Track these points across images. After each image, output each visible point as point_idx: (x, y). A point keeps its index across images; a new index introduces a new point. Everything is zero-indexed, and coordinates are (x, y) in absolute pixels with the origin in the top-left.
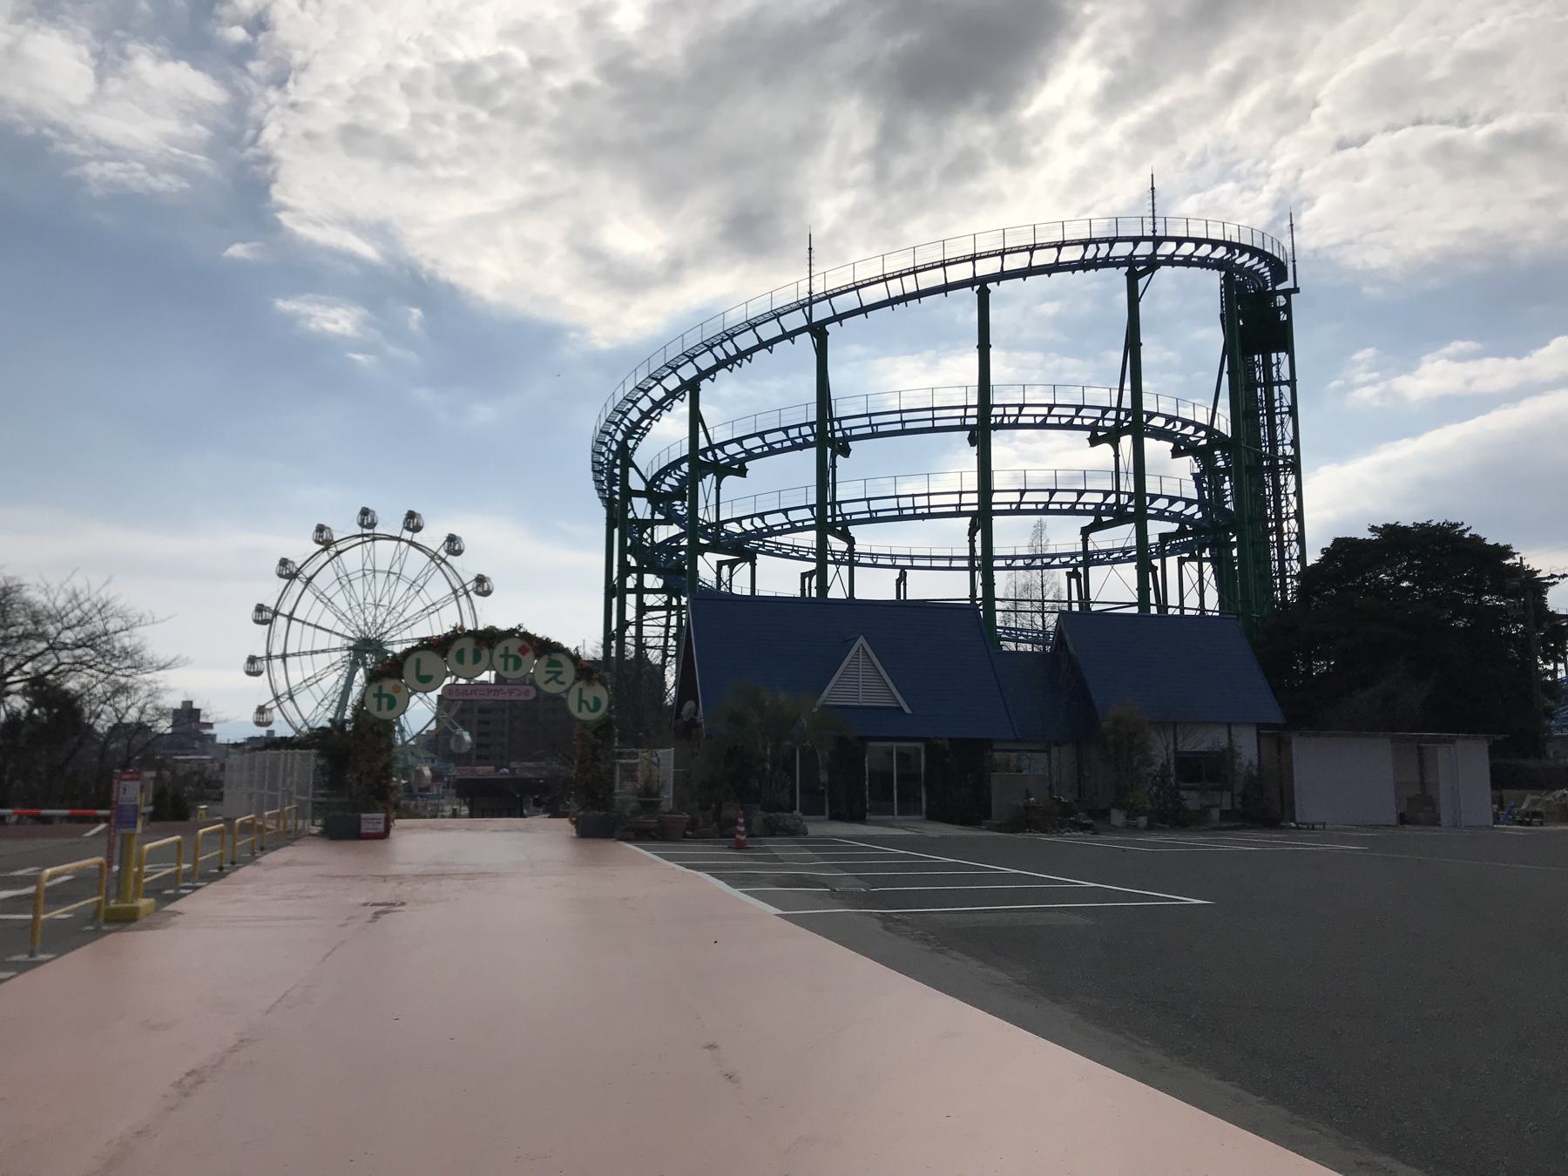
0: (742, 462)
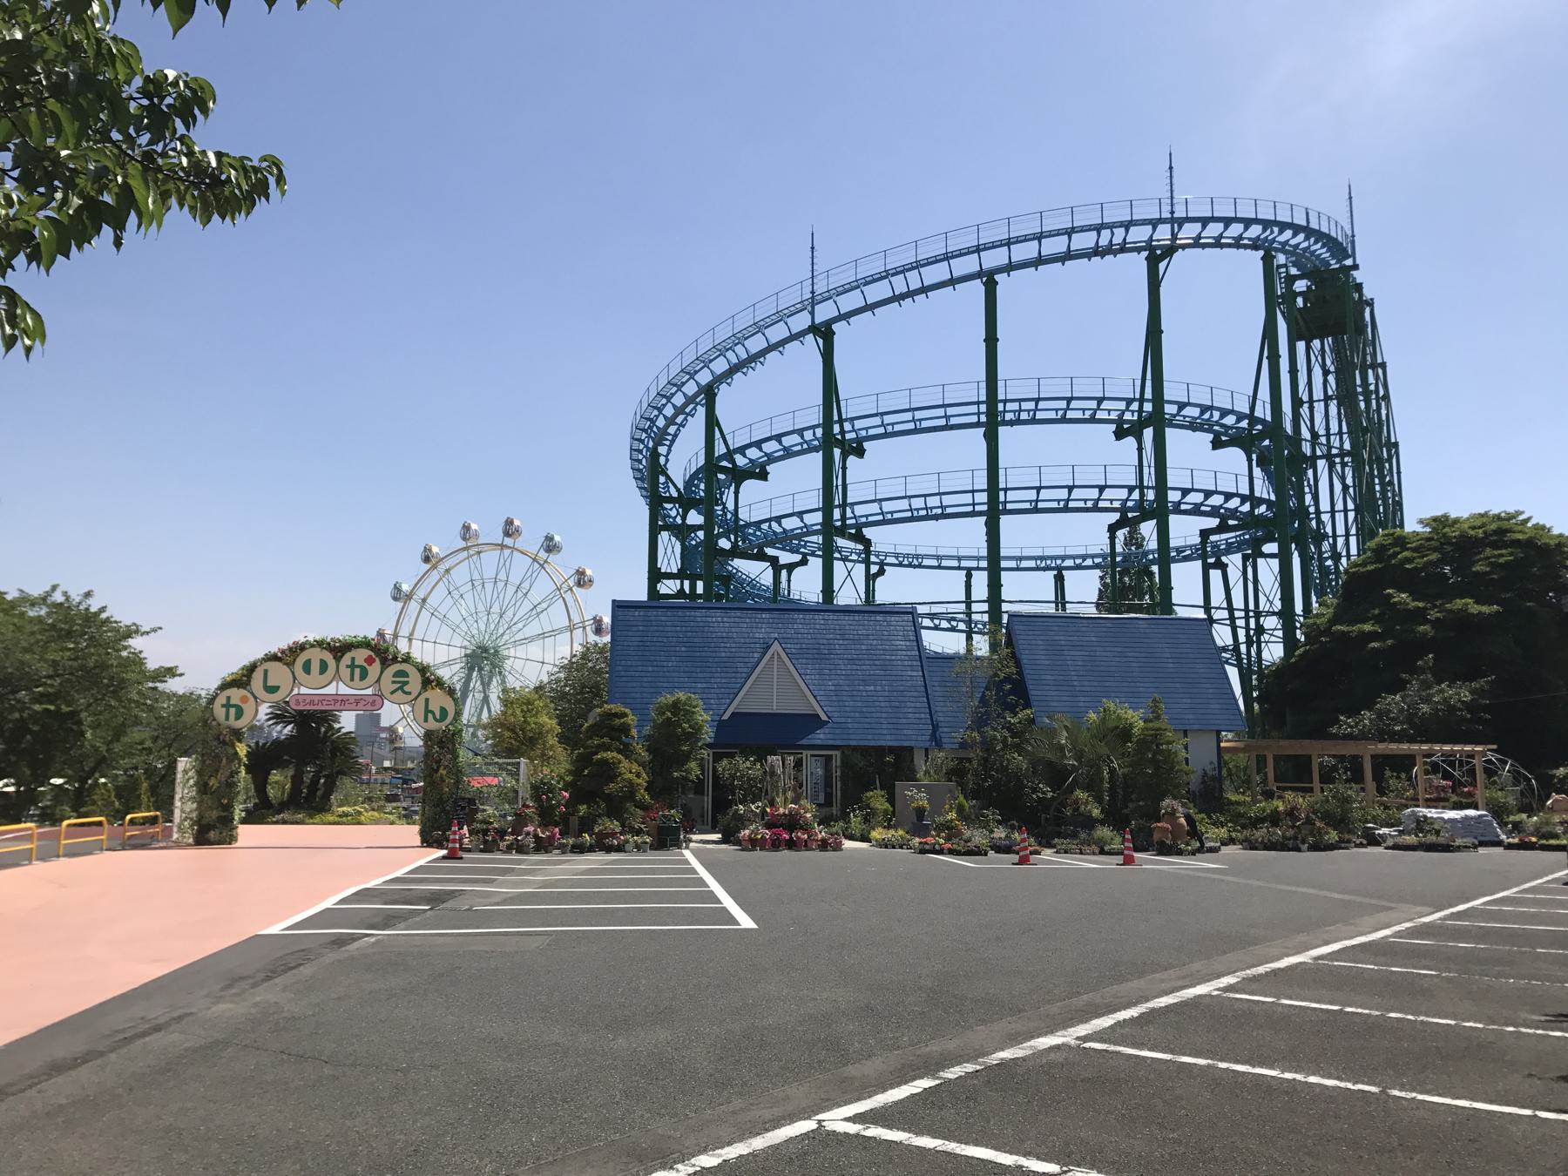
0: (763, 467)
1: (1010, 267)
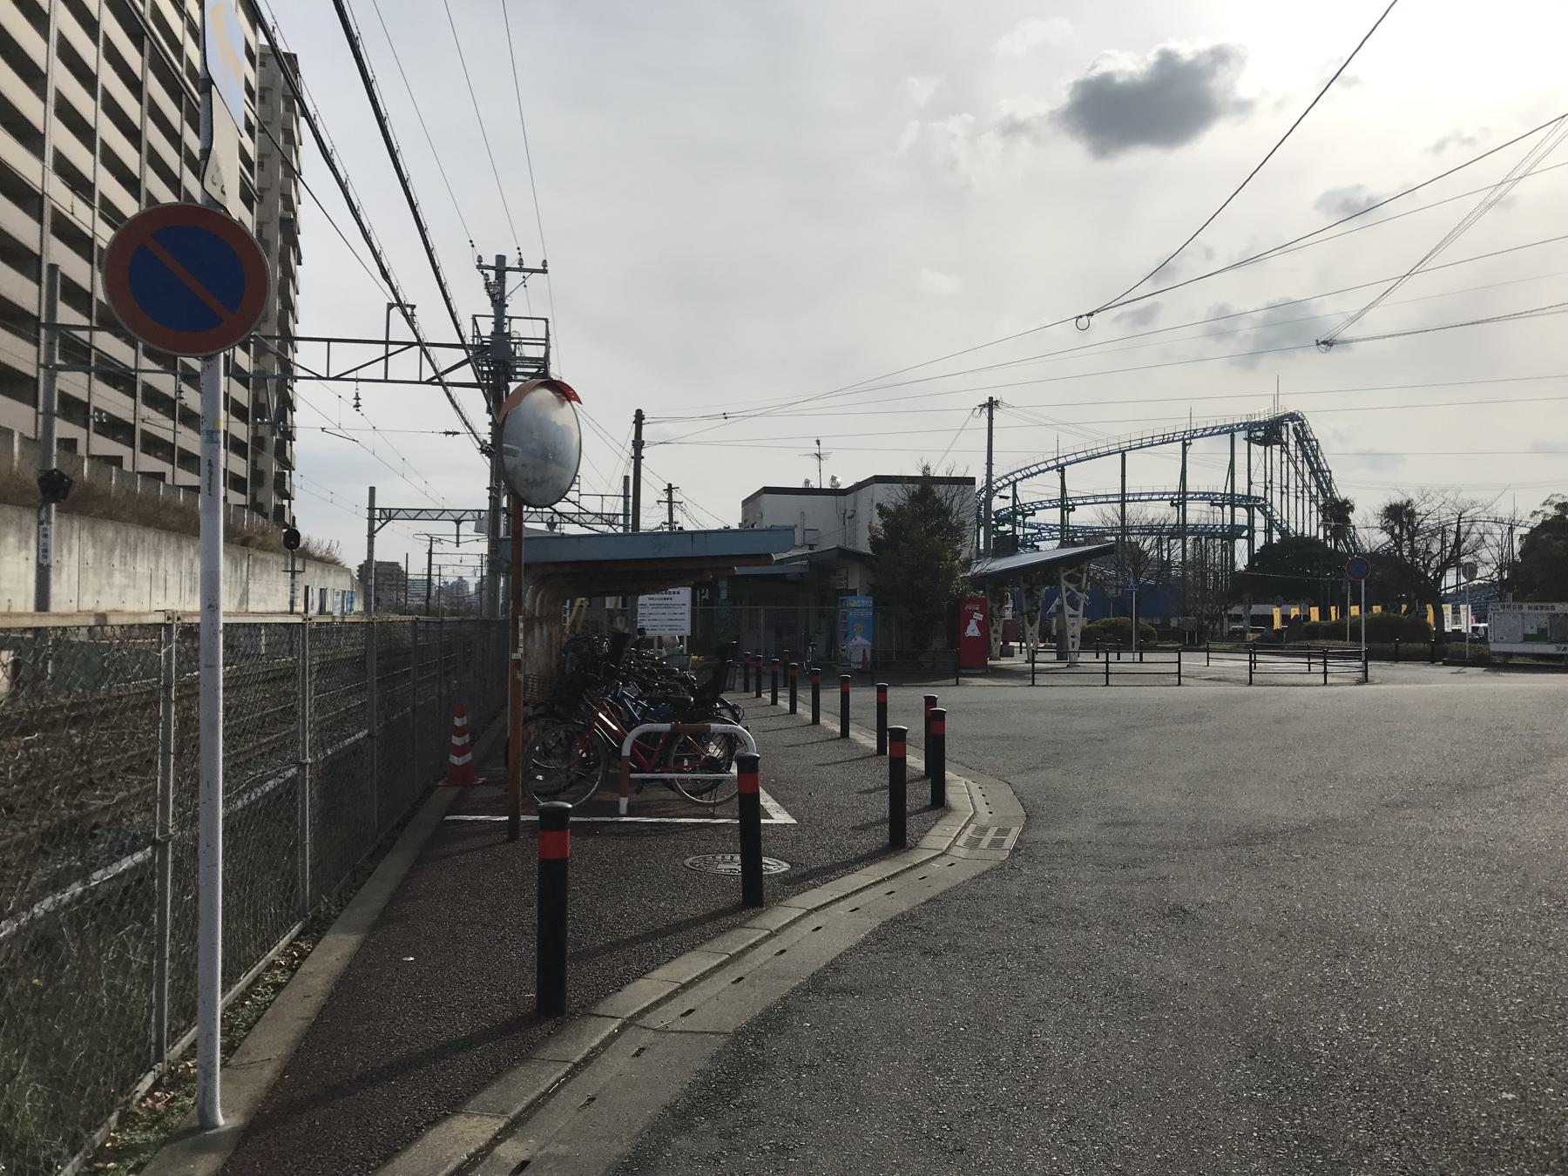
0: (1033, 511)
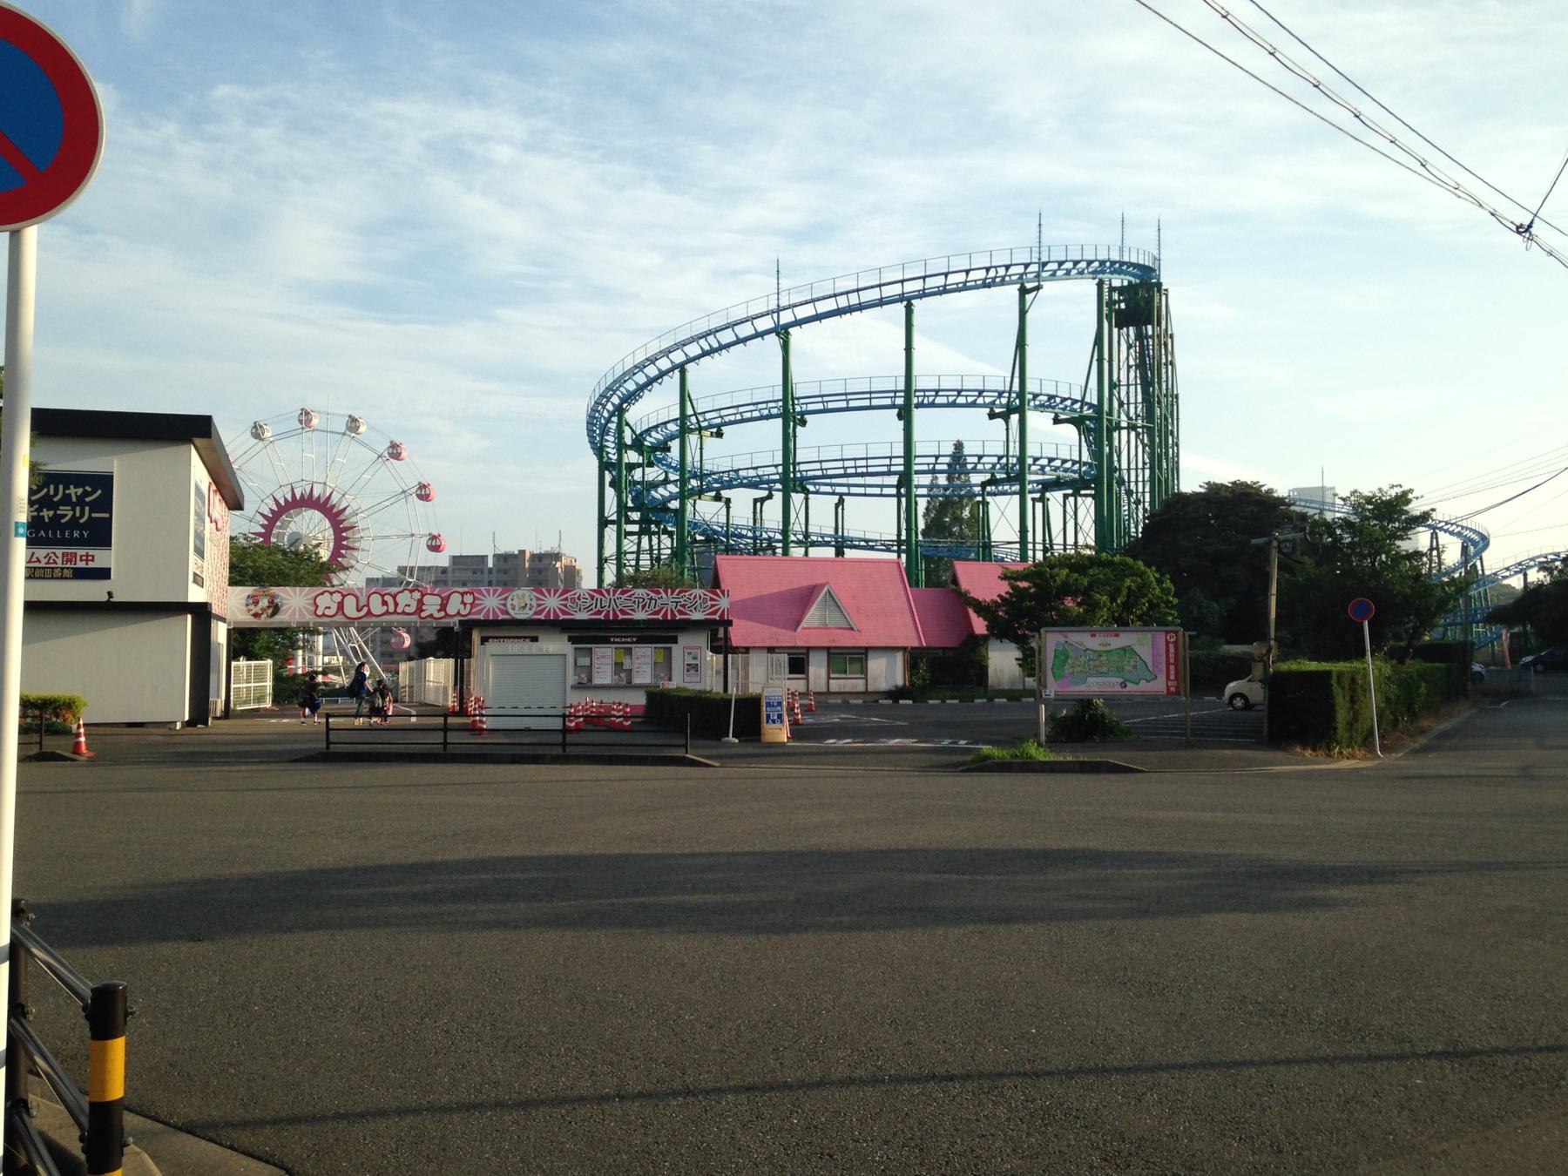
1: (923, 294)
